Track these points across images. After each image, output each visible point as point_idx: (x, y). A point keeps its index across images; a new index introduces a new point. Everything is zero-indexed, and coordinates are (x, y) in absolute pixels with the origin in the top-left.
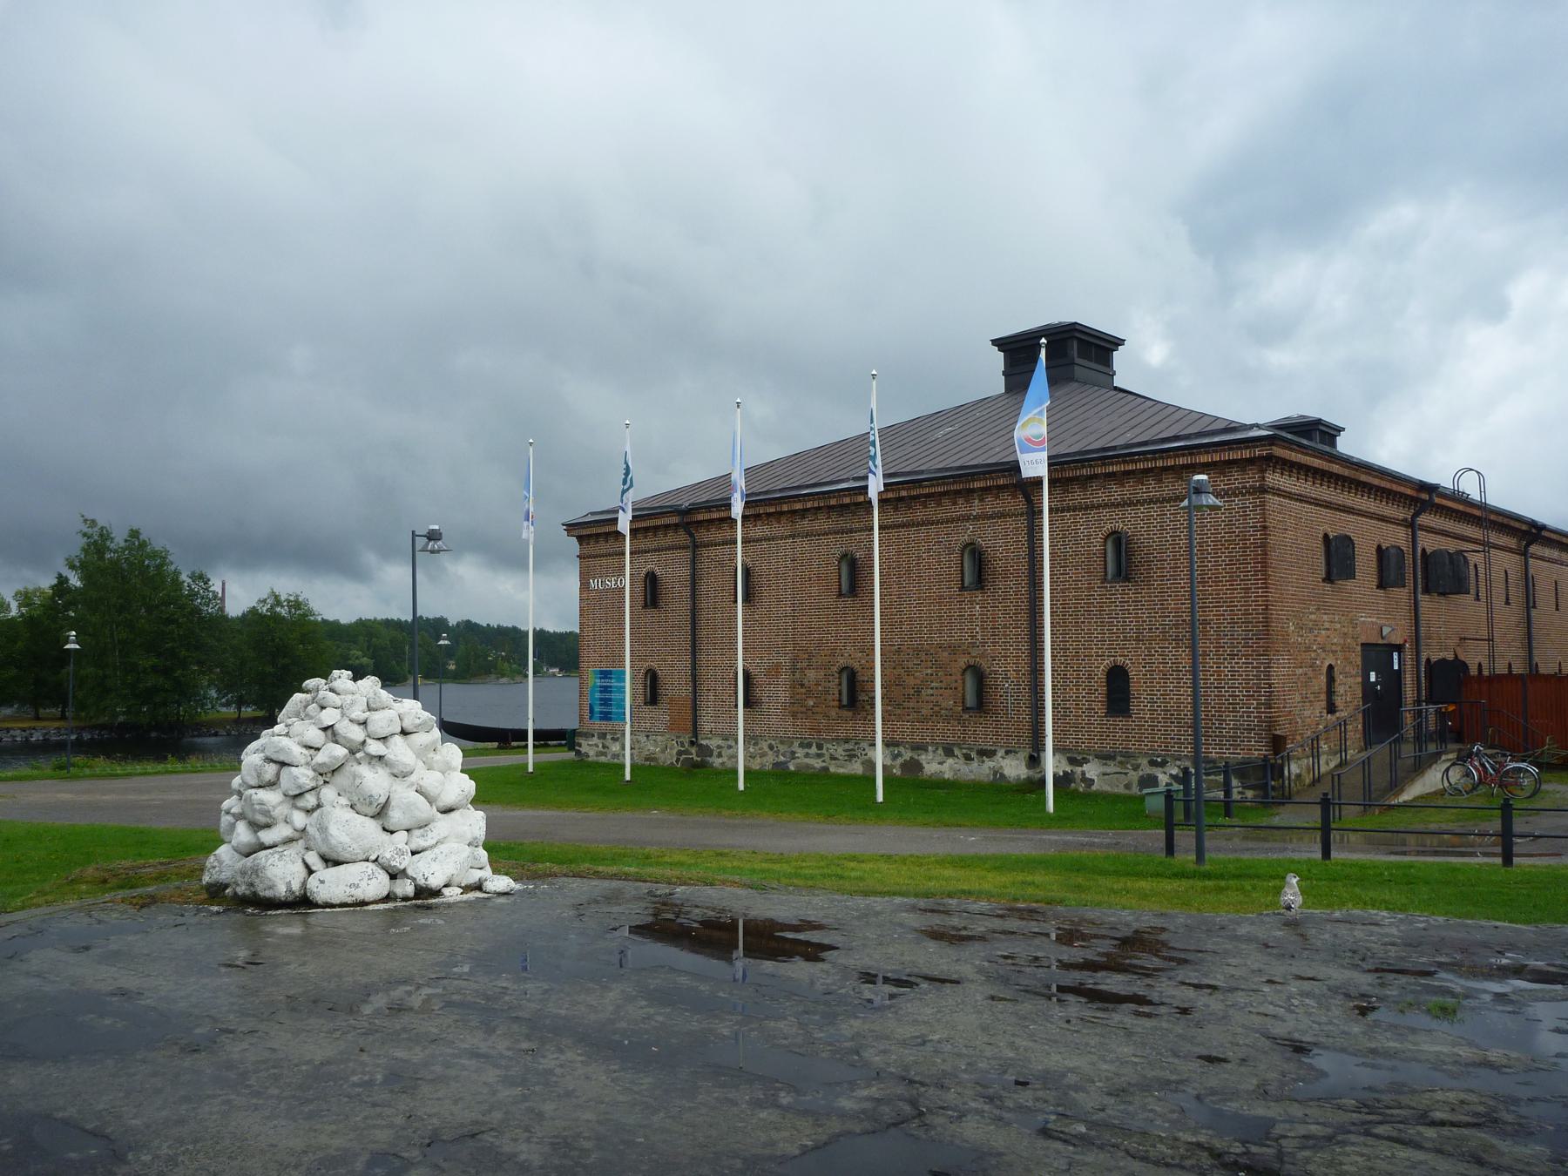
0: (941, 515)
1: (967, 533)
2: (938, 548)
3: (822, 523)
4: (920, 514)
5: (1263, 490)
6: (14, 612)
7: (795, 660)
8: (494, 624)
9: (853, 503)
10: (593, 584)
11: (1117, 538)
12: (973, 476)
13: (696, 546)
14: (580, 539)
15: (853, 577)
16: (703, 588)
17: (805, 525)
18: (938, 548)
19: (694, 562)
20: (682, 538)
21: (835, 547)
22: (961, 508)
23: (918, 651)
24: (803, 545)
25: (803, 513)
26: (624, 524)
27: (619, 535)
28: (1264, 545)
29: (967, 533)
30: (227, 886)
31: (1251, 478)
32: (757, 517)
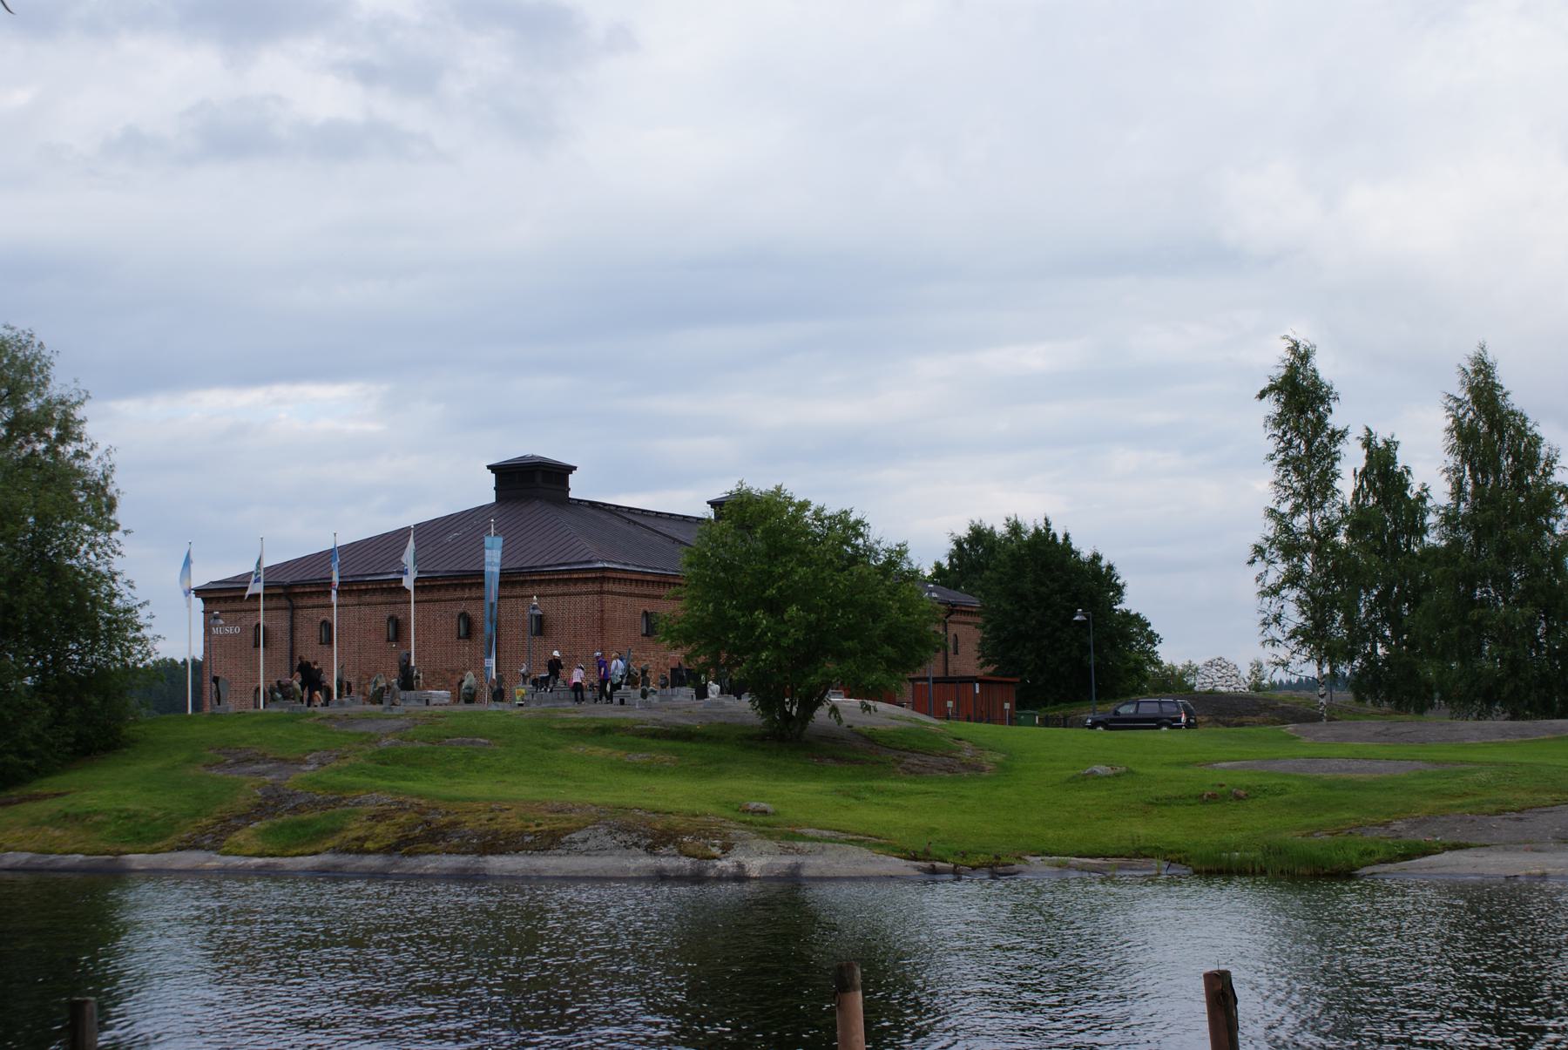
0: (448, 596)
1: (462, 607)
2: (446, 615)
3: (378, 598)
4: (436, 596)
5: (601, 593)
6: (1432, 539)
7: (360, 679)
8: (1084, 548)
9: (324, 587)
10: (215, 631)
11: (464, 616)
12: (466, 577)
13: (293, 609)
14: (205, 600)
15: (397, 630)
16: (298, 635)
17: (367, 598)
18: (446, 615)
19: (292, 618)
20: (284, 603)
21: (386, 612)
22: (459, 594)
23: (434, 673)
24: (367, 610)
25: (366, 591)
26: (257, 588)
27: (396, 588)
28: (602, 619)
29: (462, 607)
30: (1458, 421)
31: (596, 587)
32: (350, 592)
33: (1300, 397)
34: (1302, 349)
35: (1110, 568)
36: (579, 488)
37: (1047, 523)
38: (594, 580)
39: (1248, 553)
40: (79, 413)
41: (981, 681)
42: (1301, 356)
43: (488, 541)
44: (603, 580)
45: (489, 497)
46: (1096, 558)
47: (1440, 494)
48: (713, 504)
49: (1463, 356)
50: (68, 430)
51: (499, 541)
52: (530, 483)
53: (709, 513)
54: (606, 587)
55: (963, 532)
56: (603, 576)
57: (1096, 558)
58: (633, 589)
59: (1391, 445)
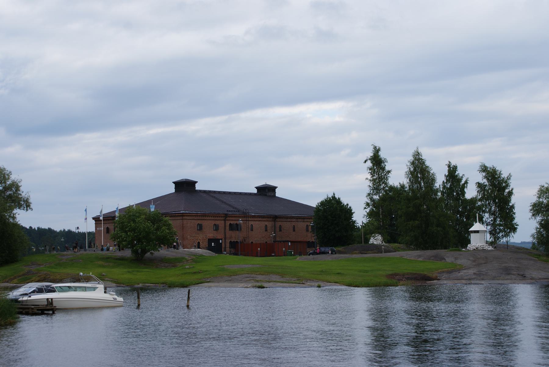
5: (183, 219)
26: (101, 218)
29: (199, 222)
33: (377, 162)
34: (377, 148)
35: (350, 207)
36: (198, 187)
37: (334, 194)
38: (181, 216)
39: (364, 206)
40: (20, 185)
41: (291, 242)
42: (377, 151)
43: (151, 206)
44: (183, 216)
45: (173, 191)
46: (31, 227)
47: (487, 183)
48: (256, 188)
49: (412, 151)
50: (18, 188)
51: (154, 206)
52: (185, 187)
53: (255, 191)
54: (184, 218)
55: (330, 196)
56: (183, 215)
57: (31, 227)
58: (194, 218)
59: (455, 168)
